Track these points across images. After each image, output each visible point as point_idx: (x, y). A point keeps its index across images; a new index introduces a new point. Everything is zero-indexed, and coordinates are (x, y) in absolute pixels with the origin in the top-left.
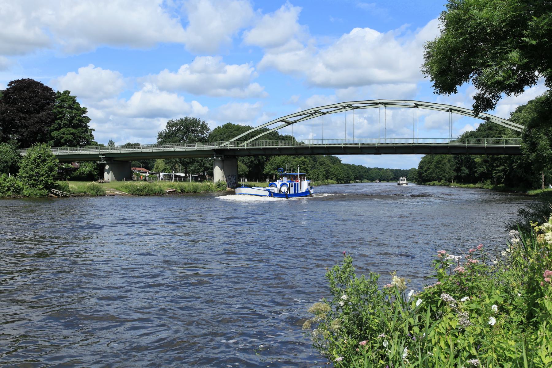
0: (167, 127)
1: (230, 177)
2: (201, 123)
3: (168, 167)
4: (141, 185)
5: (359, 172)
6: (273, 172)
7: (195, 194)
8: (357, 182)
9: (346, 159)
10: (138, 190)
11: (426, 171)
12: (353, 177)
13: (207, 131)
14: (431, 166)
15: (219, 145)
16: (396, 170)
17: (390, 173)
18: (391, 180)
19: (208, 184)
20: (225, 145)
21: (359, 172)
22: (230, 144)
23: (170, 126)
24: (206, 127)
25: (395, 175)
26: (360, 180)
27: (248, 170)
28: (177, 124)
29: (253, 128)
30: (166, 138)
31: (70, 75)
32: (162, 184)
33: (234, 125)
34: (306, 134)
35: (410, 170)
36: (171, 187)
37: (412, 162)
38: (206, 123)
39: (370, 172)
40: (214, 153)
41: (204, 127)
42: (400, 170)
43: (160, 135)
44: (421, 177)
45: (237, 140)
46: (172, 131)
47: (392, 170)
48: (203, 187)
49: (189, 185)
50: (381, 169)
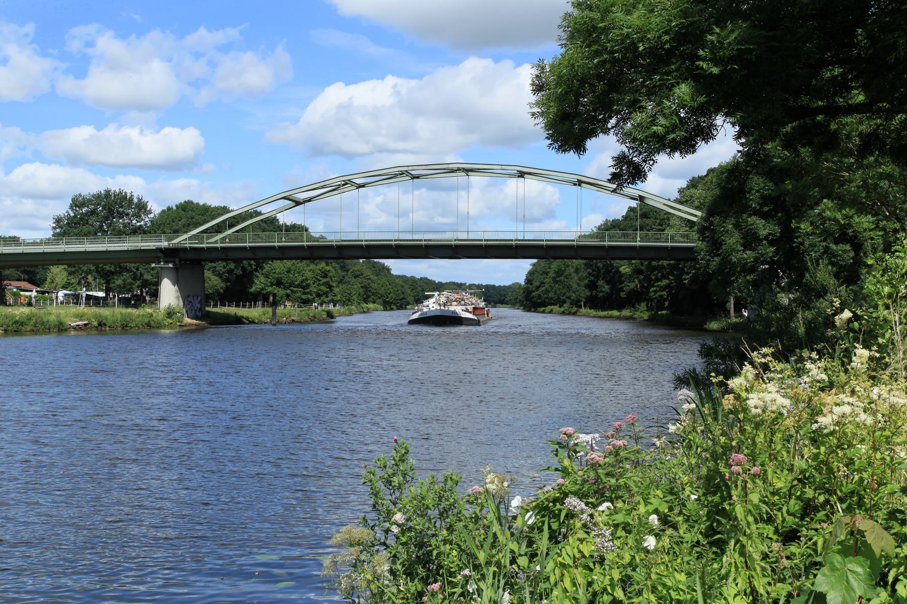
0: (71, 207)
1: (191, 299)
2: (135, 200)
10: (16, 322)
11: (538, 288)
15: (169, 240)
19: (149, 311)
20: (182, 240)
22: (190, 238)
23: (76, 206)
27: (223, 285)
28: (90, 201)
29: (232, 211)
30: (68, 227)
32: (62, 312)
33: (198, 204)
34: (325, 223)
35: (510, 287)
38: (145, 199)
41: (142, 207)
42: (494, 286)
43: (58, 221)
44: (530, 298)
48: (139, 316)
49: (115, 312)
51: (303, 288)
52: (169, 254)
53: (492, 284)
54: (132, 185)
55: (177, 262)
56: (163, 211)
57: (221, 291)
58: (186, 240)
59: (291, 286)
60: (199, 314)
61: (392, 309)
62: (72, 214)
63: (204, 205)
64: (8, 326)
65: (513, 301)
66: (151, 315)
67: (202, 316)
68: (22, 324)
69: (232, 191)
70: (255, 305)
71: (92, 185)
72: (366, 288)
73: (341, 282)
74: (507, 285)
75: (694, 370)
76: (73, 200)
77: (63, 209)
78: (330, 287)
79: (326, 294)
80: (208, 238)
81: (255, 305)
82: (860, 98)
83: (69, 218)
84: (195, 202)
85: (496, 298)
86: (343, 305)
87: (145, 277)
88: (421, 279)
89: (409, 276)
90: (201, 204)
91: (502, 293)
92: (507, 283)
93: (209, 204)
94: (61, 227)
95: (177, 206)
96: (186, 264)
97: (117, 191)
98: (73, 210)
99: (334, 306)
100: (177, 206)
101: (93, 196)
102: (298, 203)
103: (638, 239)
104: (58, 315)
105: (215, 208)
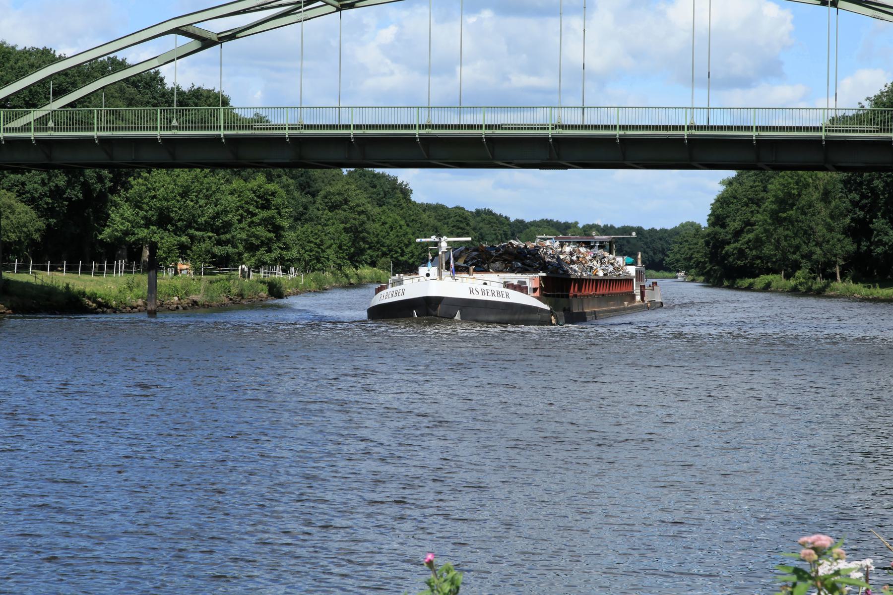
6: (142, 233)
11: (738, 234)
27: (41, 224)
29: (61, 59)
35: (675, 232)
44: (720, 257)
51: (217, 231)
57: (36, 236)
59: (189, 226)
72: (356, 233)
74: (669, 226)
79: (267, 245)
81: (110, 267)
86: (305, 271)
88: (478, 212)
89: (450, 205)
91: (658, 245)
99: (285, 271)
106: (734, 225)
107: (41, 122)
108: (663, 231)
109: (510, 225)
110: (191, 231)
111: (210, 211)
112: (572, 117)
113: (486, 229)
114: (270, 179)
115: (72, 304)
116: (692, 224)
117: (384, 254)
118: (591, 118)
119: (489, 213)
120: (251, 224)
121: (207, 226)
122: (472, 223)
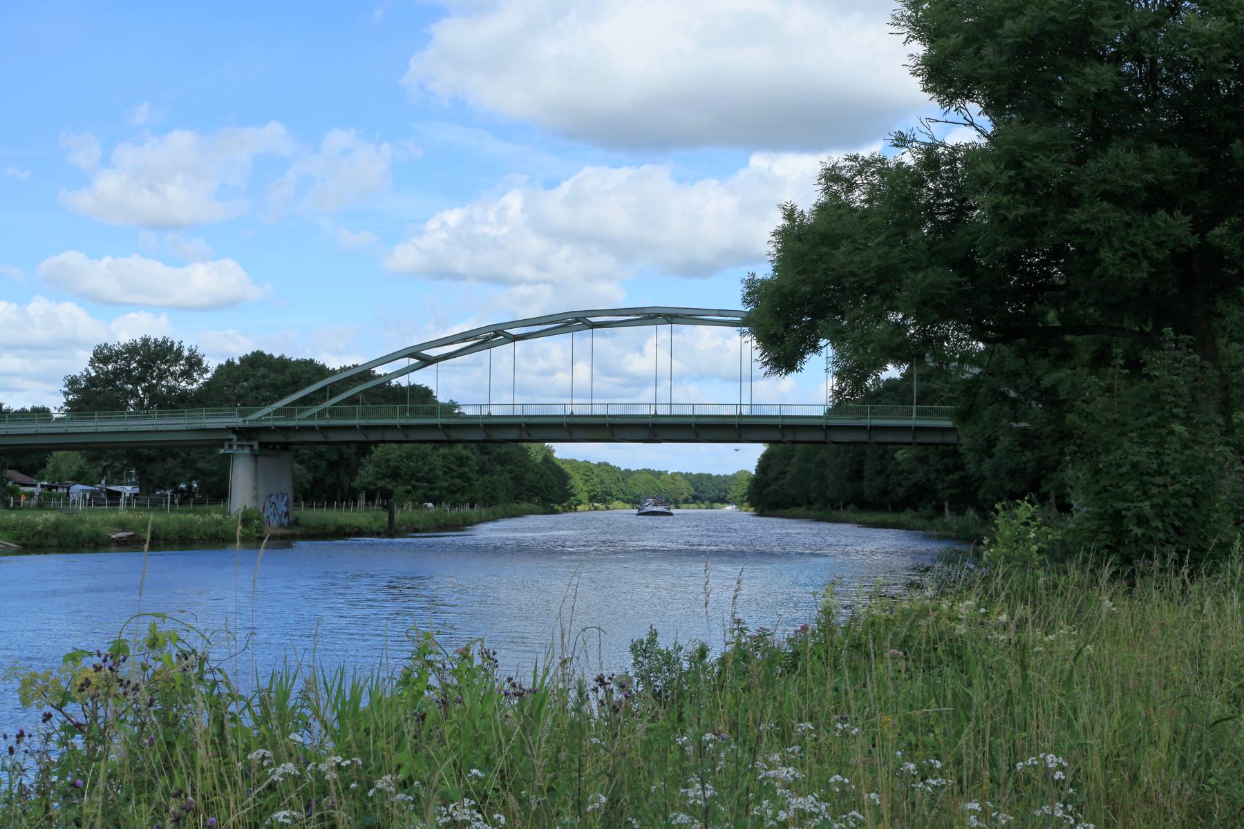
0: (92, 363)
1: (273, 499)
2: (186, 353)
3: (94, 472)
4: (46, 520)
5: (602, 482)
6: (381, 483)
7: (182, 541)
8: (596, 509)
9: (563, 451)
10: (39, 532)
11: (776, 479)
12: (584, 496)
13: (201, 375)
14: (789, 468)
15: (244, 414)
16: (700, 476)
17: (684, 485)
18: (686, 501)
19: (218, 516)
20: (263, 415)
21: (602, 482)
22: (276, 412)
23: (100, 361)
24: (199, 362)
25: (705, 491)
26: (603, 501)
27: (310, 477)
28: (118, 354)
29: (334, 372)
30: (90, 395)
31: (857, 601)
32: (98, 518)
33: (271, 356)
34: (471, 388)
35: (734, 477)
36: (123, 526)
37: (745, 458)
38: (200, 352)
39: (630, 481)
40: (234, 437)
41: (194, 363)
42: (709, 476)
43: (73, 382)
44: (768, 494)
45: (293, 404)
46: (108, 372)
47: (687, 476)
48: (204, 524)
49: (172, 518)
50: (658, 474)
51: (428, 481)
52: (244, 434)
53: (706, 472)
54: (186, 338)
55: (256, 447)
56: (220, 367)
57: (307, 485)
58: (269, 414)
59: (412, 478)
60: (285, 521)
61: (555, 512)
62: (93, 374)
63: (281, 358)
64: (28, 539)
65: (739, 499)
66: (219, 523)
67: (289, 524)
68: (47, 536)
69: (338, 341)
70: (355, 506)
71: (125, 331)
72: (518, 479)
73: (482, 471)
74: (730, 473)
75: (367, 505)
76: (95, 353)
77: (80, 364)
78: (468, 480)
79: (462, 490)
80: (300, 411)
81: (355, 506)
82: (900, 455)
83: (91, 381)
84: (267, 353)
85: (713, 495)
86: (484, 506)
87: (199, 465)
88: (599, 464)
89: (581, 460)
90: (276, 356)
91: (723, 486)
92: (730, 471)
93: (288, 356)
94: (75, 391)
95: (241, 359)
96: (269, 445)
97: (160, 339)
98: (94, 367)
99: (472, 507)
100: (241, 359)
101: (125, 346)
102: (413, 353)
103: (914, 415)
104: (93, 524)
105: (298, 361)
106: (772, 474)
107: (321, 414)
108: (726, 476)
109: (622, 473)
110: (413, 482)
111: (427, 468)
112: (663, 411)
113: (605, 476)
114: (465, 448)
115: (549, 551)
116: (745, 472)
117: (537, 494)
118: (676, 411)
119: (607, 464)
120: (452, 477)
121: (423, 479)
122: (596, 472)
